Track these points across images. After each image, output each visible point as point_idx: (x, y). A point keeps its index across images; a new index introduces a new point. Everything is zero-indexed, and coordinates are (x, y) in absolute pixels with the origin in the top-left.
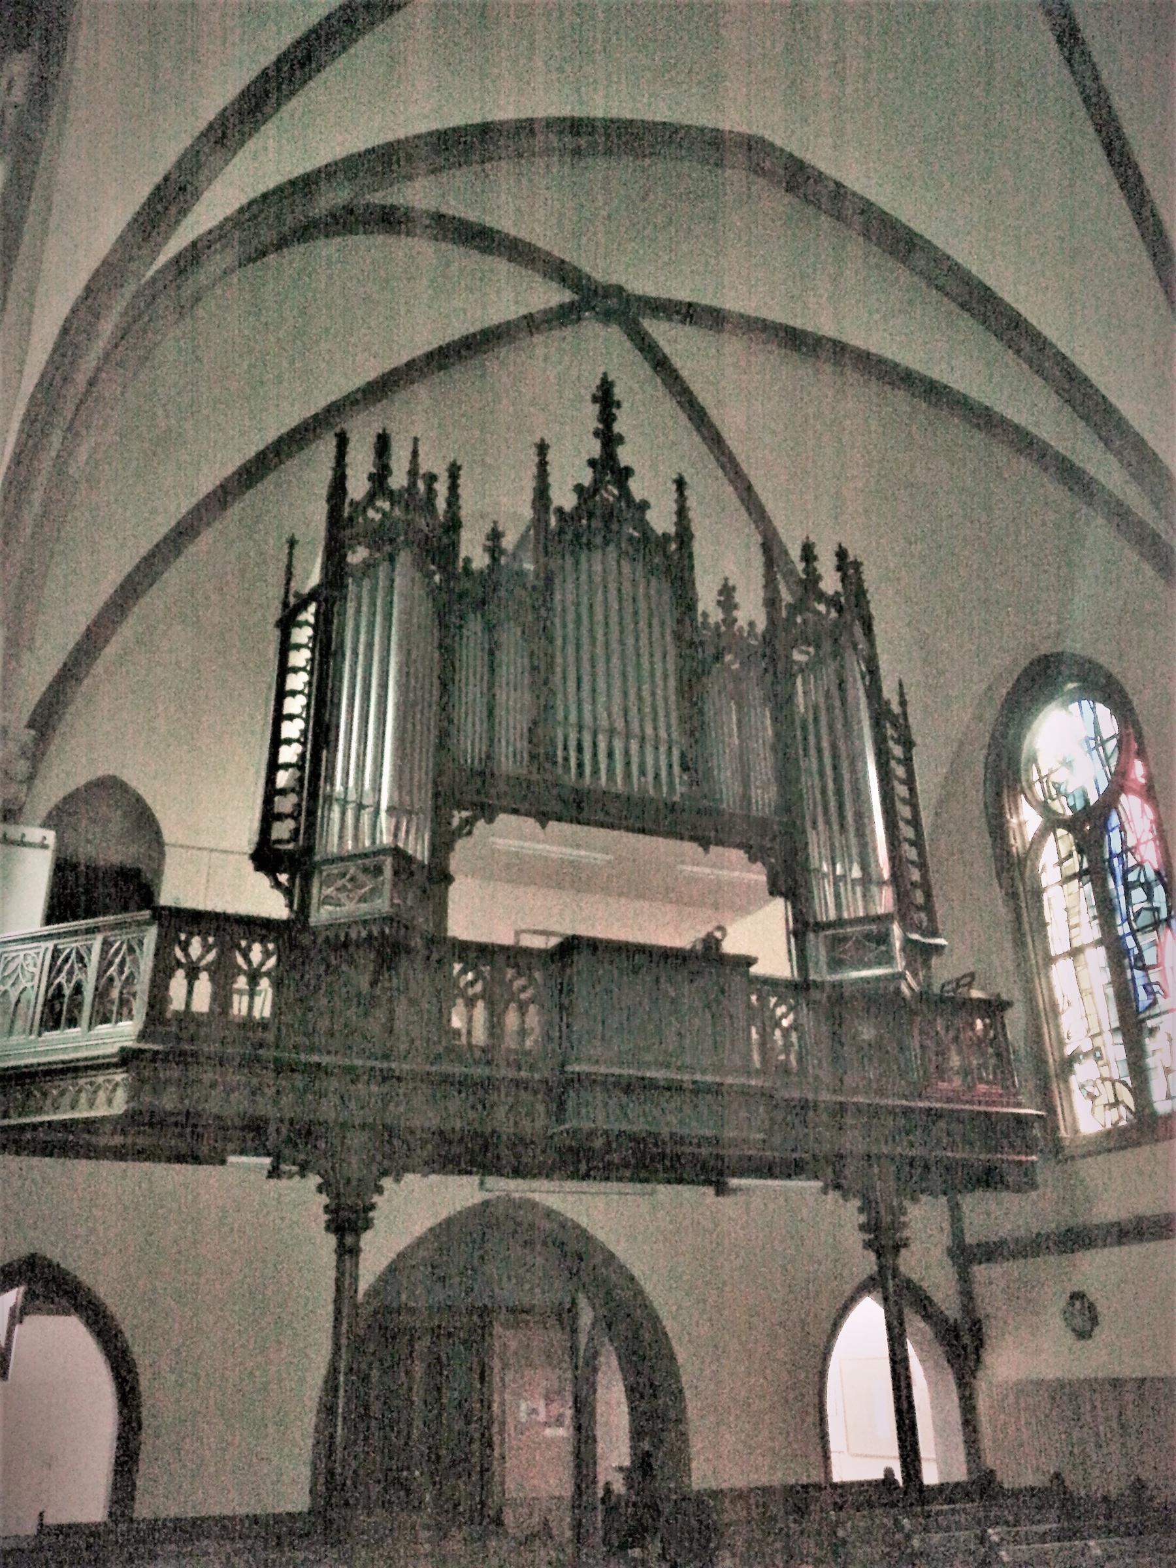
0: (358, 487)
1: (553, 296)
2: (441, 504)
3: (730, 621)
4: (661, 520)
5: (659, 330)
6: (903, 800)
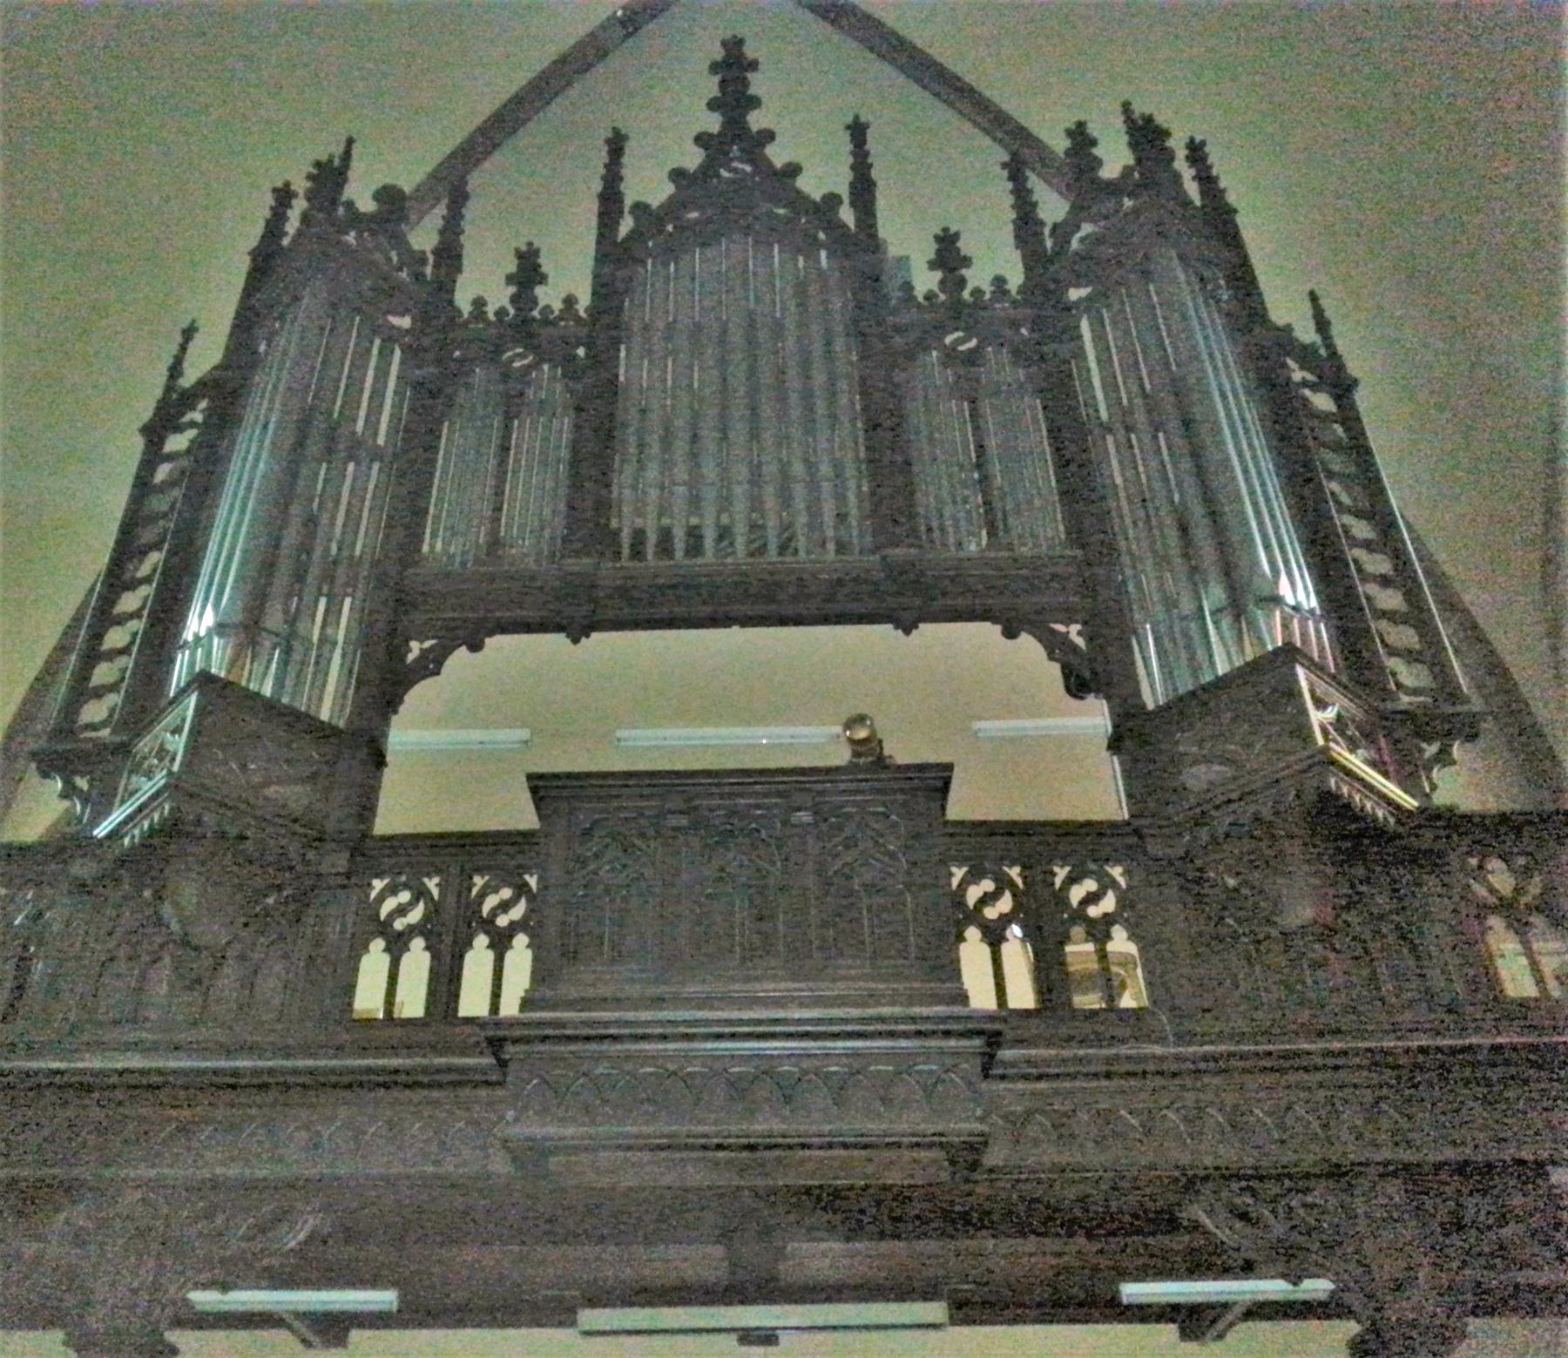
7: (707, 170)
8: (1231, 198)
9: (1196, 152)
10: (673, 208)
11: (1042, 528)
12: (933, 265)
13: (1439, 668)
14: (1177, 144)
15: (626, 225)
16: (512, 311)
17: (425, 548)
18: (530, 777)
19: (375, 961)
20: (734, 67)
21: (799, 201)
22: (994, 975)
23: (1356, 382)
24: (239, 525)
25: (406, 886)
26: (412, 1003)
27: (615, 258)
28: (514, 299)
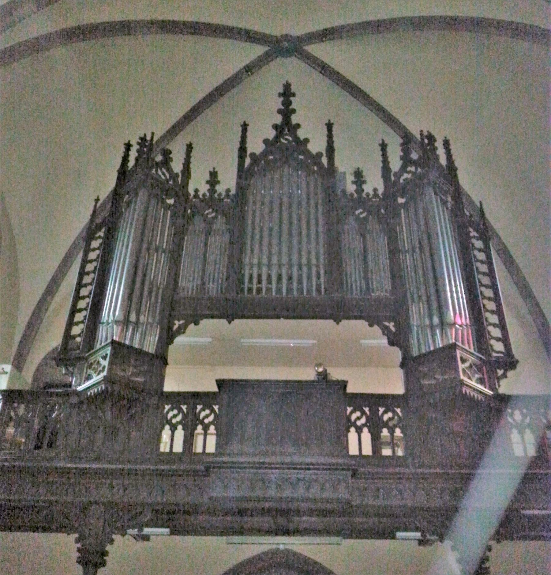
0: (395, 164)
1: (258, 50)
3: (360, 190)
4: (317, 146)
5: (315, 49)
6: (484, 274)
7: (277, 138)
8: (456, 164)
9: (446, 143)
10: (265, 154)
11: (382, 286)
12: (353, 183)
14: (439, 144)
15: (248, 161)
16: (208, 194)
17: (180, 285)
18: (217, 381)
20: (287, 94)
21: (307, 153)
22: (360, 443)
23: (517, 362)
25: (176, 408)
26: (178, 448)
27: (243, 173)
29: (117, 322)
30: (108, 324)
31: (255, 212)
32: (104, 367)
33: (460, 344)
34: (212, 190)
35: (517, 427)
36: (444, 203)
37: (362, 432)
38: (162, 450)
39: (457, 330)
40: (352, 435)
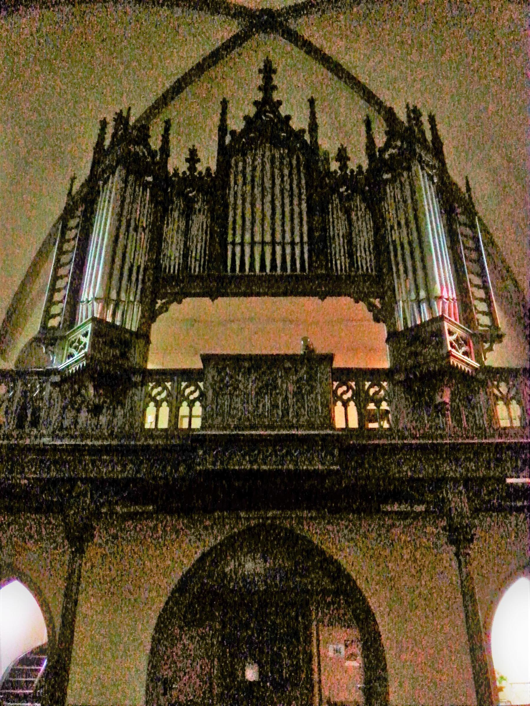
0: (380, 140)
2: (429, 136)
4: (299, 122)
7: (258, 115)
9: (432, 119)
10: (245, 132)
11: (365, 259)
13: (493, 320)
14: (425, 119)
15: (228, 139)
19: (151, 410)
20: (268, 71)
21: (290, 131)
24: (99, 264)
26: (163, 424)
28: (189, 169)
29: (96, 299)
30: (88, 302)
31: (236, 187)
32: (85, 345)
33: (446, 316)
34: (192, 169)
35: (502, 399)
36: (431, 178)
37: (193, 405)
38: (147, 426)
39: (444, 303)
40: (339, 408)
